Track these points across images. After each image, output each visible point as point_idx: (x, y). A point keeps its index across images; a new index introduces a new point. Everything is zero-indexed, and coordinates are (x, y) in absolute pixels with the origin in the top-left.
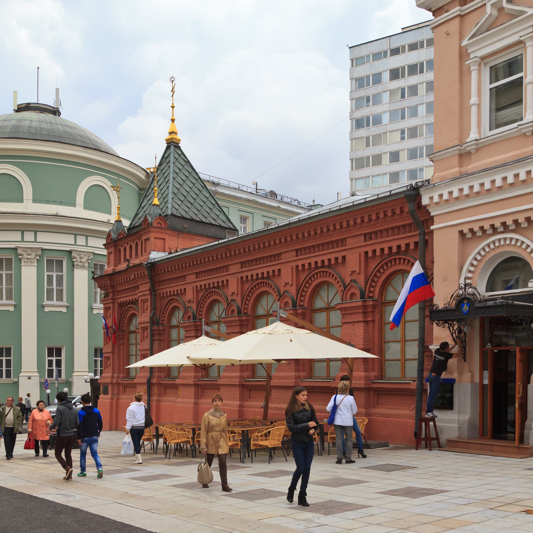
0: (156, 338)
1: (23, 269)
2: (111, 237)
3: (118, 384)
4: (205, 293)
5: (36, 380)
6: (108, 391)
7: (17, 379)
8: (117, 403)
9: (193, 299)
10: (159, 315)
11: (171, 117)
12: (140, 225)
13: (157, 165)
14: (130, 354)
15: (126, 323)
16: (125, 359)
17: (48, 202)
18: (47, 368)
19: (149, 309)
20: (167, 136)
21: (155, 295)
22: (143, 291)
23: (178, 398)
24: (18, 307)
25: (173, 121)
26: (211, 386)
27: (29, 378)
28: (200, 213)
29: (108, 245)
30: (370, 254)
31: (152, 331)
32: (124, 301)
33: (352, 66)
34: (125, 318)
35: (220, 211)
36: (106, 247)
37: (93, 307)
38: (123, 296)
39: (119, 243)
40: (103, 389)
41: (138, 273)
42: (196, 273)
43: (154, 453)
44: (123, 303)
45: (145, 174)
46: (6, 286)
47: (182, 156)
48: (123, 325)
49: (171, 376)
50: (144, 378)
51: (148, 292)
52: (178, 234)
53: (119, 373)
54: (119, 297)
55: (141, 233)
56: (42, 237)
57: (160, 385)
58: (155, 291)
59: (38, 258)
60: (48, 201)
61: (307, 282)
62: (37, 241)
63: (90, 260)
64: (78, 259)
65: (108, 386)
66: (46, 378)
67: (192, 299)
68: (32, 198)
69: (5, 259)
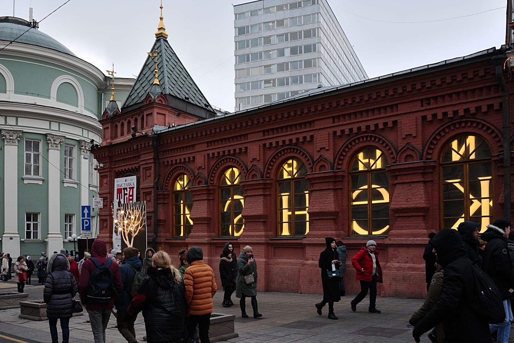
9: (205, 166)
10: (162, 181)
11: (160, 16)
12: (142, 102)
18: (26, 230)
19: (153, 176)
20: (157, 32)
25: (161, 19)
27: (11, 239)
30: (211, 156)
33: (236, 19)
37: (64, 181)
42: (208, 143)
45: (103, 77)
47: (169, 48)
51: (152, 161)
55: (142, 109)
61: (216, 166)
63: (62, 143)
67: (261, 143)
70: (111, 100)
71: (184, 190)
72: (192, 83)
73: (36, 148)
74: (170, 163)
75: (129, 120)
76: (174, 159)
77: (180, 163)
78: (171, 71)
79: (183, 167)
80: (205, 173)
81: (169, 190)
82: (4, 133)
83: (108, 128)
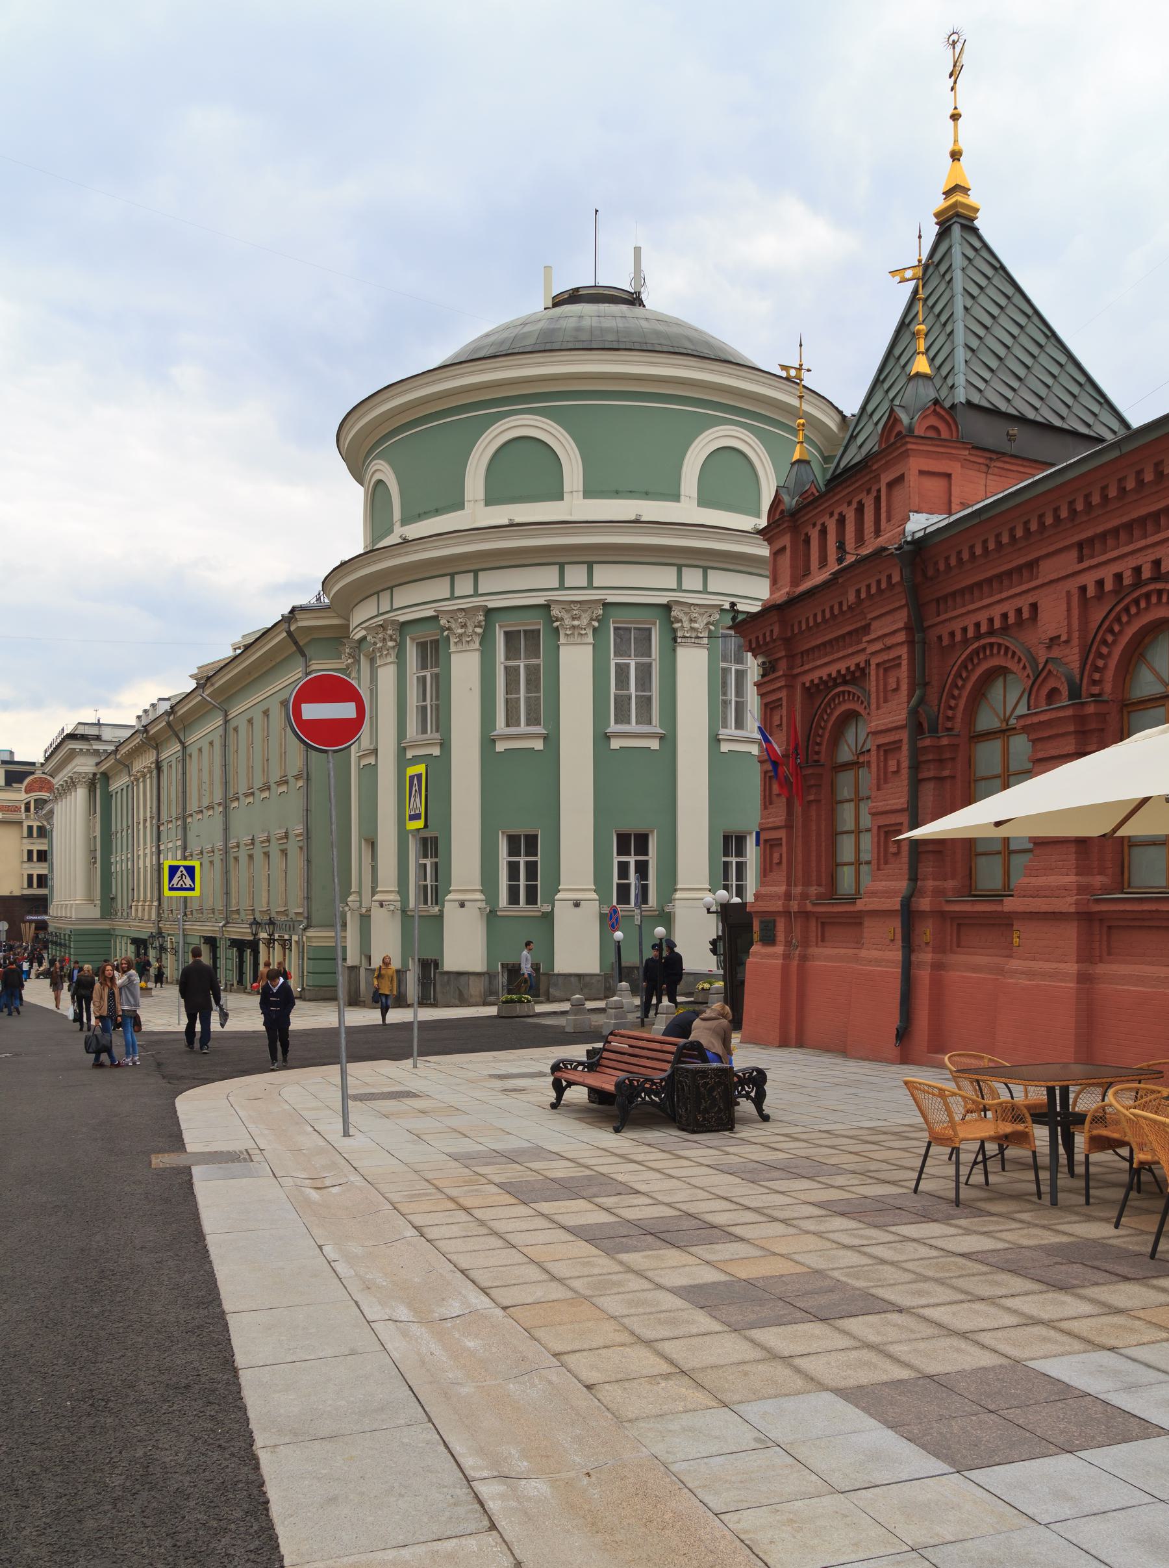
0: (929, 772)
1: (563, 650)
2: (781, 508)
3: (806, 915)
4: (1115, 605)
5: (592, 909)
6: (775, 935)
7: (550, 907)
8: (801, 969)
9: (1069, 633)
10: (936, 702)
11: (950, 147)
13: (924, 258)
14: (839, 830)
15: (825, 743)
16: (823, 844)
17: (617, 494)
18: (616, 880)
19: (904, 687)
20: (940, 203)
21: (925, 643)
22: (885, 635)
23: (1010, 956)
24: (552, 740)
26: (1143, 920)
28: (1044, 405)
29: (772, 530)
30: (1091, 591)
31: (915, 752)
32: (821, 678)
34: (824, 728)
35: (1100, 404)
36: (766, 537)
37: (721, 737)
38: (819, 663)
39: (806, 518)
40: (761, 930)
41: (867, 582)
42: (1080, 545)
43: (1039, 1194)
44: (817, 685)
45: (838, 418)
46: (527, 693)
48: (817, 748)
49: (976, 890)
50: (887, 897)
51: (901, 637)
52: (987, 462)
53: (807, 883)
54: (806, 667)
56: (605, 576)
57: (942, 915)
58: (924, 630)
59: (596, 624)
60: (617, 492)
62: (594, 586)
63: (712, 624)
64: (686, 624)
65: (774, 921)
66: (615, 903)
68: (581, 488)
69: (525, 631)
70: (794, 460)
71: (1004, 726)
72: (1063, 359)
73: (644, 647)
74: (958, 638)
75: (840, 514)
76: (969, 622)
77: (991, 632)
78: (978, 325)
79: (1000, 645)
80: (1072, 656)
81: (956, 731)
82: (558, 612)
83: (783, 549)
